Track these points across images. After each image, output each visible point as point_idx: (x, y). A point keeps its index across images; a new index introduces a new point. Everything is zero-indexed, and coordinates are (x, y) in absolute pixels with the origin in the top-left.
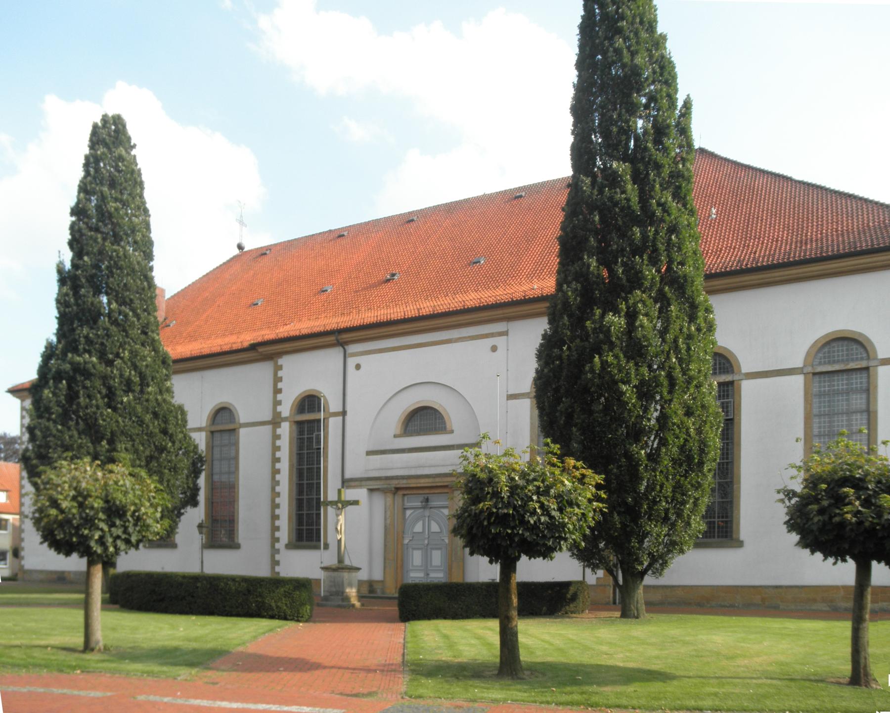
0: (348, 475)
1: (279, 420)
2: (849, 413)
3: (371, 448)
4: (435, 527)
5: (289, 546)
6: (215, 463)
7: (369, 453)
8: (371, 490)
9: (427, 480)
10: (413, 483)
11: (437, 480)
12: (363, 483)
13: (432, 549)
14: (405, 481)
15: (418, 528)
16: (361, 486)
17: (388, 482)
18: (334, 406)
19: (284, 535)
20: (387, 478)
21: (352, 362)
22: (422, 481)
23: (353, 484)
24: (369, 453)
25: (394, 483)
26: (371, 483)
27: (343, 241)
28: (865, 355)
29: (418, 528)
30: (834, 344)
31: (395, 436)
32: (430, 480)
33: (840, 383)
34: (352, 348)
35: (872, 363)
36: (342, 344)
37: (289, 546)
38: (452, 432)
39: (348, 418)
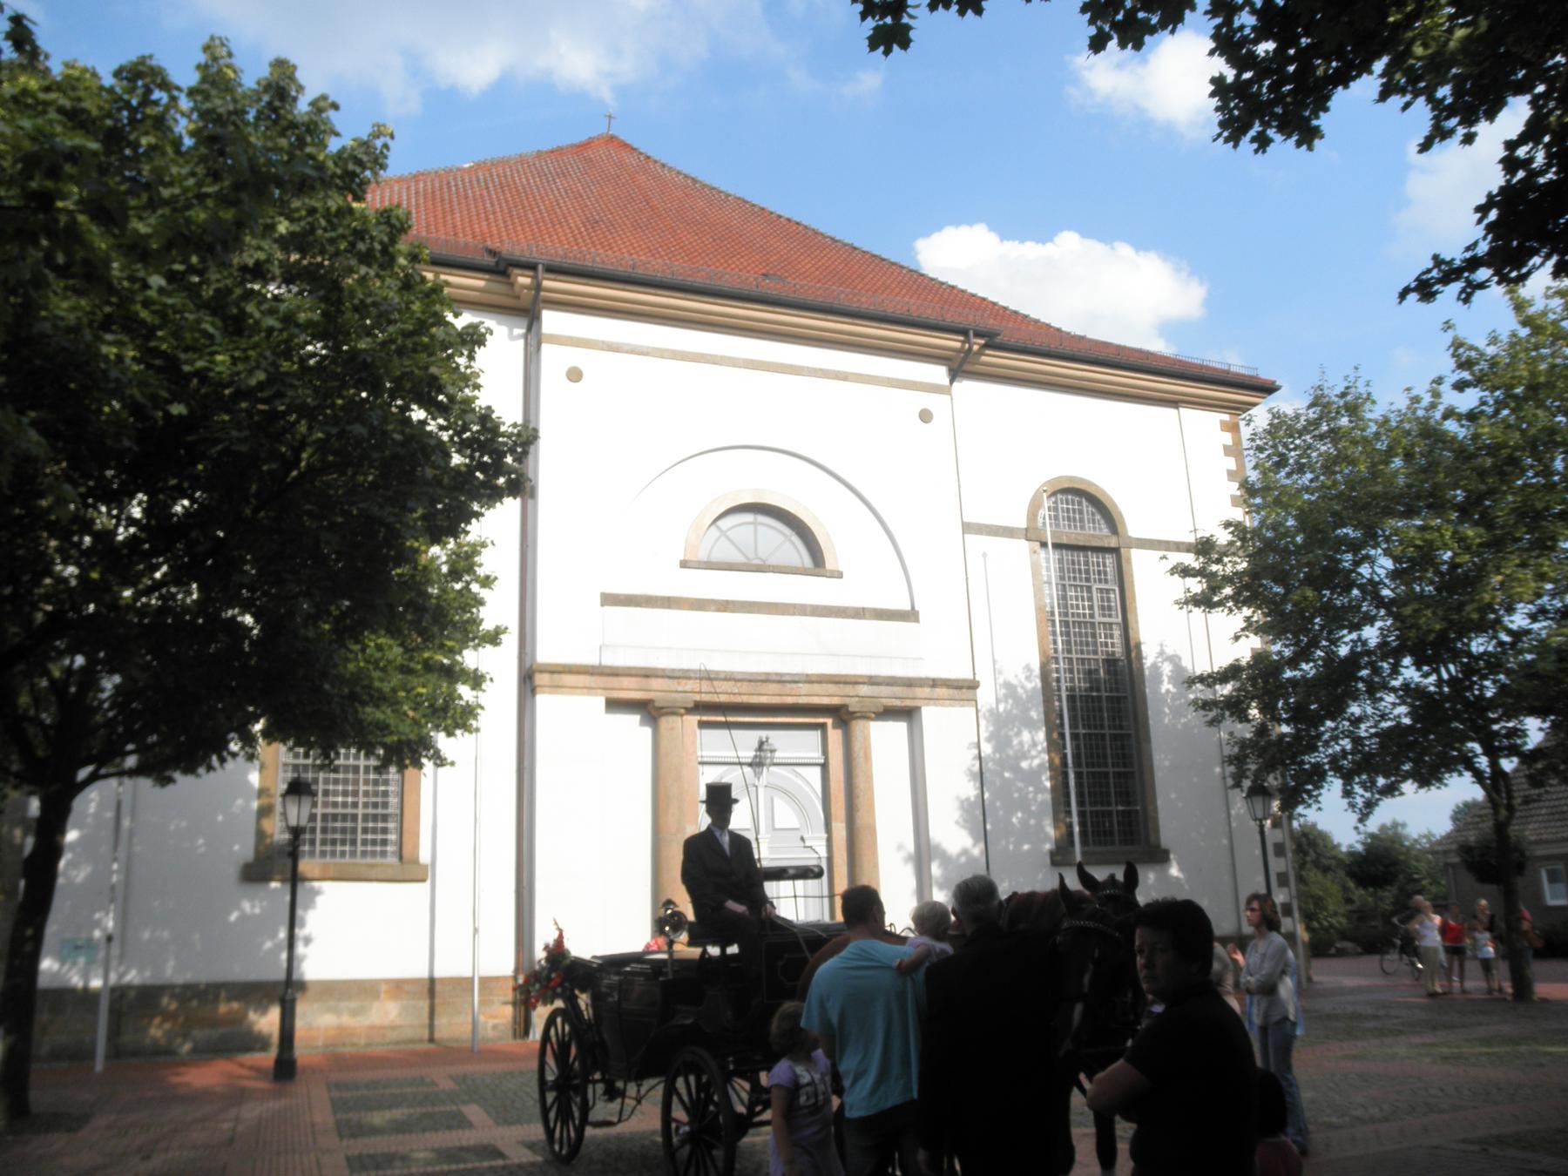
7: (609, 600)
17: (849, 690)
21: (553, 359)
23: (569, 679)
24: (609, 600)
34: (552, 321)
38: (840, 575)
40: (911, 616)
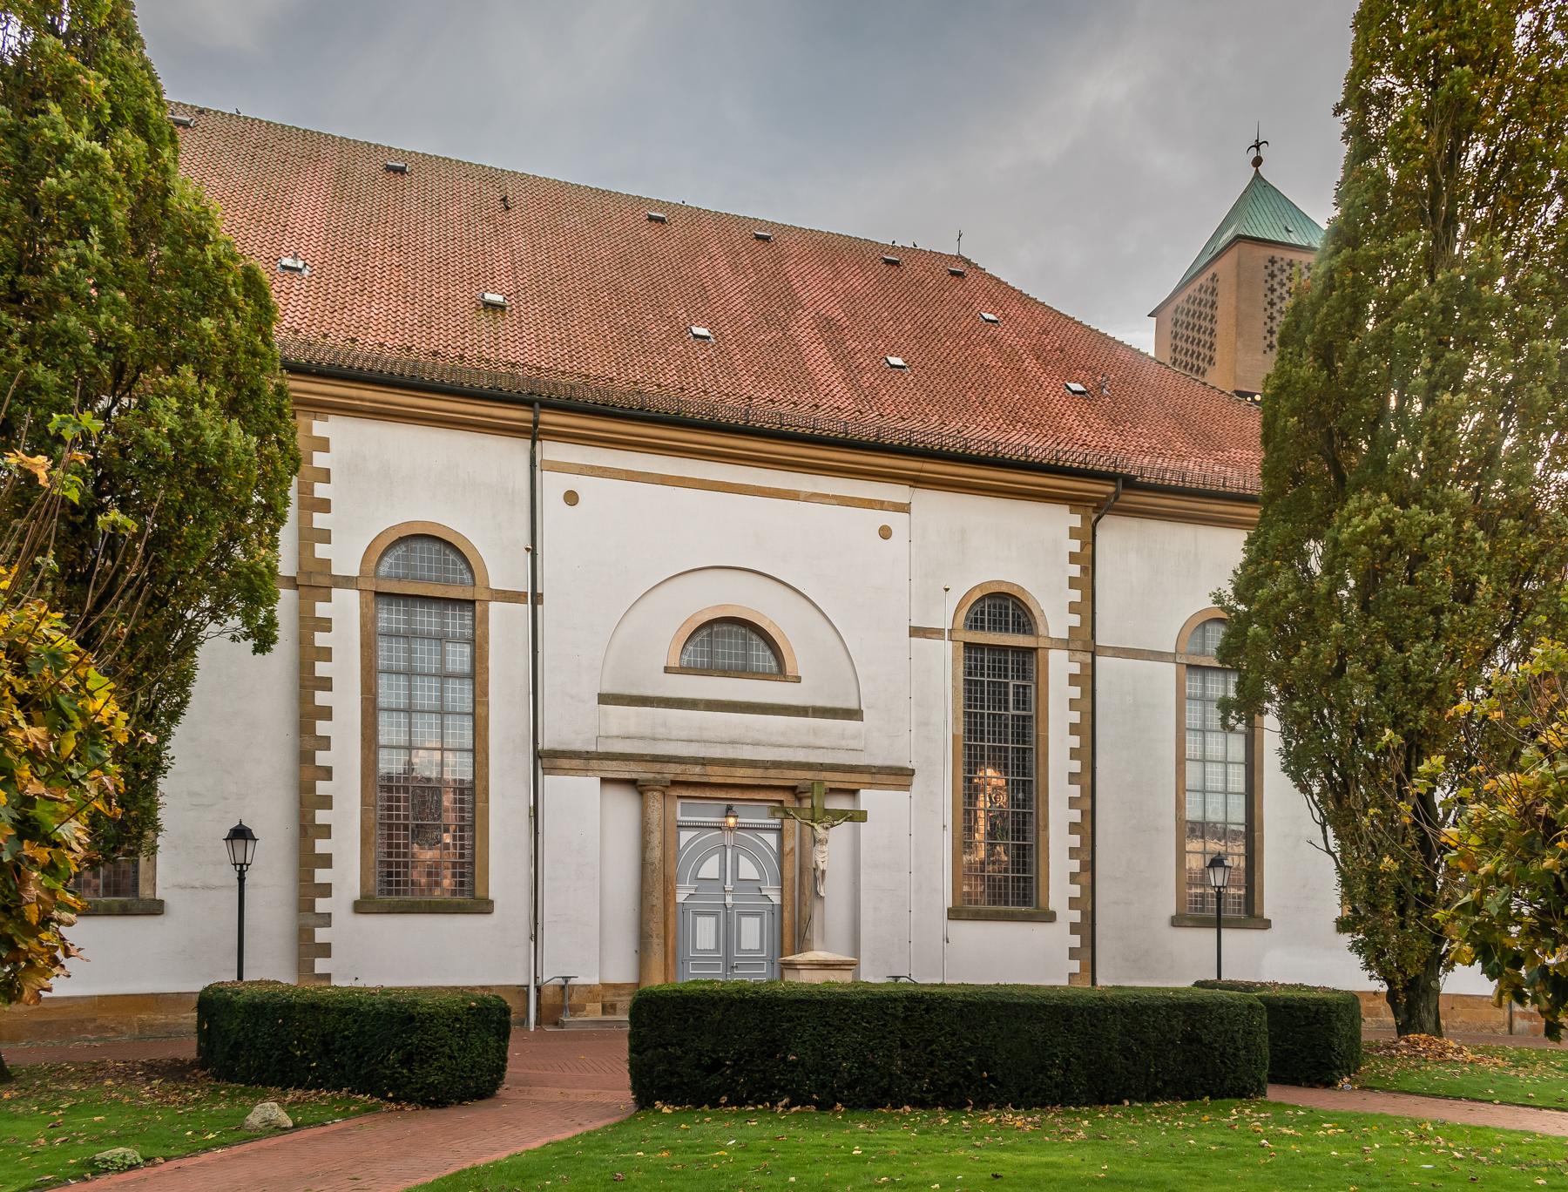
0: (547, 743)
1: (324, 581)
2: (444, 676)
3: (608, 688)
4: (748, 870)
5: (360, 907)
6: (1189, 737)
7: (604, 699)
8: (604, 781)
9: (749, 772)
10: (717, 775)
11: (772, 773)
12: (594, 764)
13: (741, 914)
14: (698, 769)
15: (710, 869)
16: (585, 771)
17: (657, 767)
18: (501, 566)
19: (347, 871)
20: (656, 759)
22: (741, 772)
23: (565, 763)
24: (604, 699)
25: (672, 771)
26: (613, 765)
27: (763, 251)
28: (467, 576)
29: (710, 869)
30: (417, 545)
31: (667, 670)
32: (759, 772)
33: (427, 619)
34: (551, 451)
35: (479, 594)
36: (534, 434)
37: (360, 907)
39: (546, 610)
40: (853, 714)
